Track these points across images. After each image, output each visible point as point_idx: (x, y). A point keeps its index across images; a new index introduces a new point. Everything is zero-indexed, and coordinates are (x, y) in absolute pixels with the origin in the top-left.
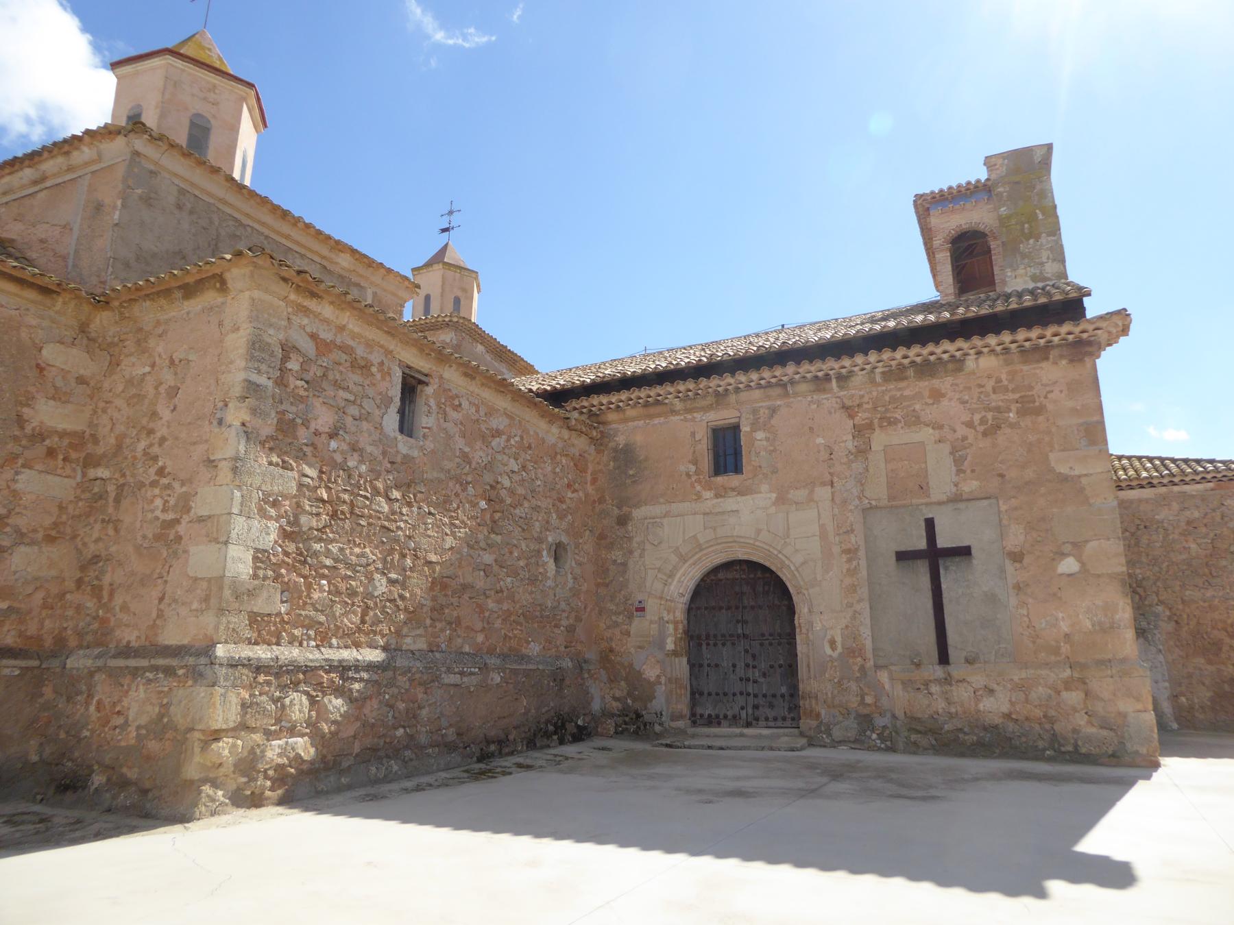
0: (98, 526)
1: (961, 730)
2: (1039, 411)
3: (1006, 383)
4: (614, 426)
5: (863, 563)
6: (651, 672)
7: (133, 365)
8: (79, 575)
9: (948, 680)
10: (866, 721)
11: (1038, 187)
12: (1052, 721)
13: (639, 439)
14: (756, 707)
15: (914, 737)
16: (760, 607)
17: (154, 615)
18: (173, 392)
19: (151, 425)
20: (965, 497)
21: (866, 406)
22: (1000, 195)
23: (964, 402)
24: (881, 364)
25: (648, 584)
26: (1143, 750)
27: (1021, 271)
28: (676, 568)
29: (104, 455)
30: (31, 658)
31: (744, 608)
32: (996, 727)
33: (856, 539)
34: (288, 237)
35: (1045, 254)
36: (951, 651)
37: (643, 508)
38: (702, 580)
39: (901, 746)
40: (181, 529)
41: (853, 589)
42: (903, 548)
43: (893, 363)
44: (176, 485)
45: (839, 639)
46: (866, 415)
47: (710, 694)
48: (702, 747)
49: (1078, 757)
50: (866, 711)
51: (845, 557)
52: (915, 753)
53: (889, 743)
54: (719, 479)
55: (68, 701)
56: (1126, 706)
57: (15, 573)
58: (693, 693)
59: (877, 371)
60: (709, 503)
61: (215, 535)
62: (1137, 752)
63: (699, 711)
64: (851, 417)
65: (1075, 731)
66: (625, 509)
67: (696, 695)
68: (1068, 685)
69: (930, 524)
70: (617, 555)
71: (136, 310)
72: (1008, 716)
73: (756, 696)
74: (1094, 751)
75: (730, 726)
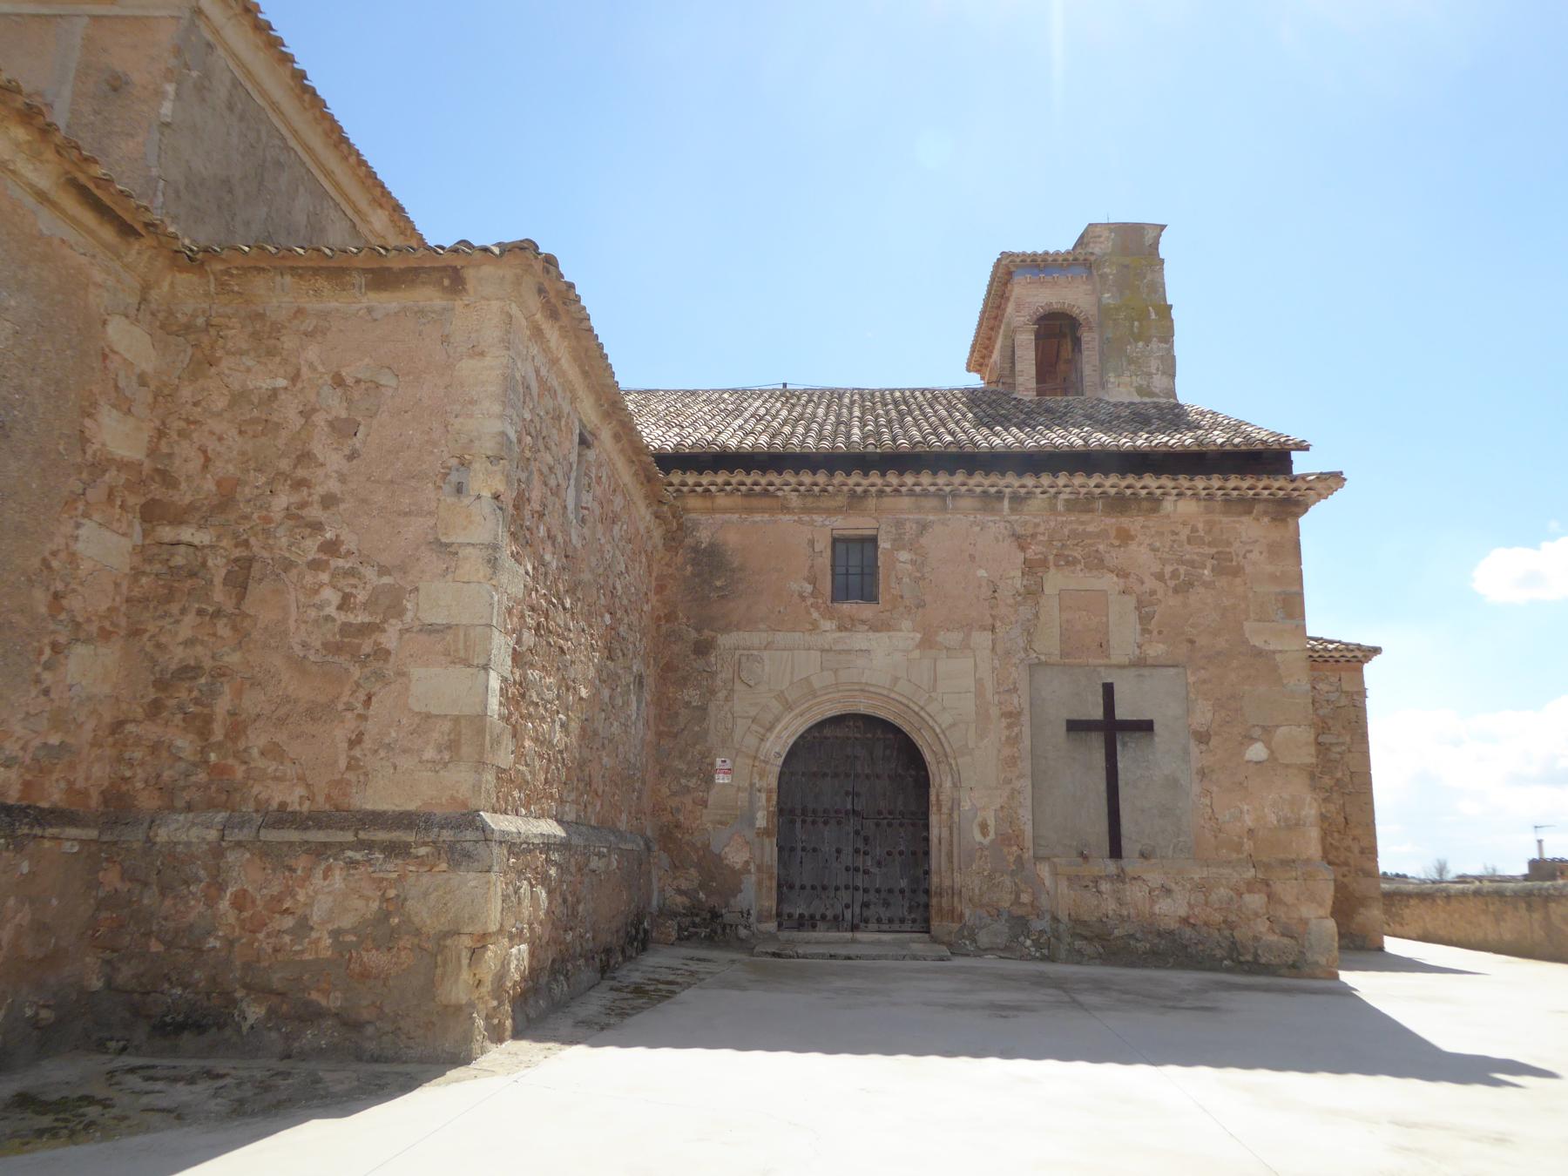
0: (190, 619)
1: (1132, 936)
2: (1237, 571)
3: (1202, 533)
4: (693, 516)
5: (1026, 730)
6: (736, 857)
7: (249, 370)
8: (152, 694)
9: (1120, 877)
10: (1020, 924)
11: (1149, 277)
12: (1232, 926)
13: (732, 539)
14: (865, 905)
15: (1078, 944)
16: (878, 777)
17: (343, 764)
18: (344, 429)
19: (301, 473)
20: (1149, 661)
21: (1041, 538)
22: (1103, 277)
23: (1155, 550)
24: (1068, 490)
25: (737, 737)
26: (1323, 961)
27: (1125, 379)
28: (777, 720)
29: (191, 508)
30: (86, 826)
31: (857, 776)
32: (1171, 933)
33: (1019, 701)
34: (328, 174)
35: (1154, 364)
36: (1124, 842)
37: (734, 634)
38: (802, 737)
39: (1063, 954)
40: (389, 639)
41: (1012, 761)
42: (1075, 717)
43: (1083, 490)
44: (370, 573)
45: (991, 823)
46: (1040, 548)
47: (803, 887)
48: (822, 956)
49: (1256, 967)
50: (1020, 911)
51: (1004, 722)
52: (1079, 963)
53: (1045, 951)
54: (846, 607)
55: (163, 894)
56: (1309, 911)
57: (70, 687)
58: (779, 886)
59: (1062, 496)
60: (830, 637)
61: (462, 654)
62: (1317, 963)
63: (787, 909)
64: (1023, 548)
65: (1256, 938)
66: (707, 633)
67: (785, 887)
68: (1250, 887)
69: (1108, 690)
70: (692, 695)
71: (259, 284)
72: (1185, 921)
73: (866, 891)
74: (1274, 961)
75: (828, 930)
